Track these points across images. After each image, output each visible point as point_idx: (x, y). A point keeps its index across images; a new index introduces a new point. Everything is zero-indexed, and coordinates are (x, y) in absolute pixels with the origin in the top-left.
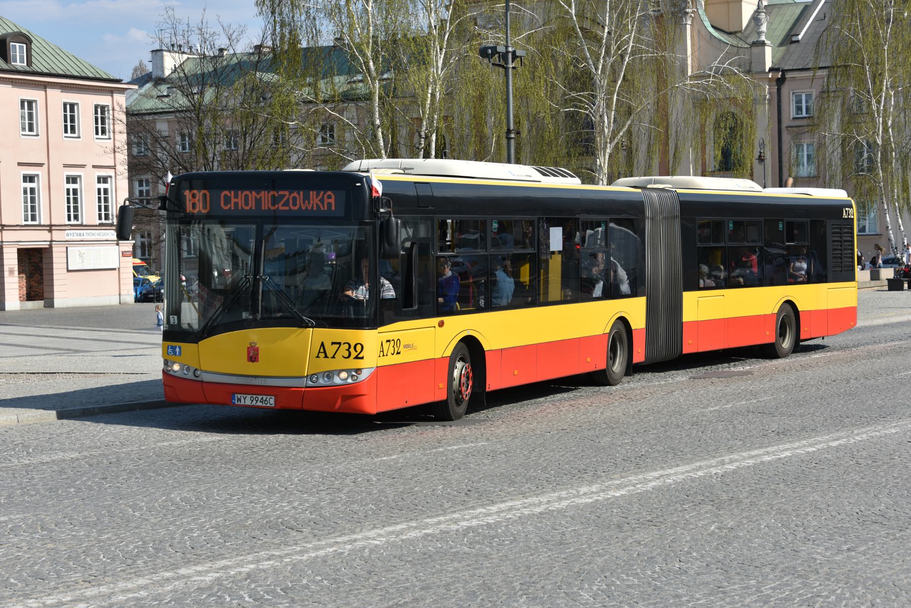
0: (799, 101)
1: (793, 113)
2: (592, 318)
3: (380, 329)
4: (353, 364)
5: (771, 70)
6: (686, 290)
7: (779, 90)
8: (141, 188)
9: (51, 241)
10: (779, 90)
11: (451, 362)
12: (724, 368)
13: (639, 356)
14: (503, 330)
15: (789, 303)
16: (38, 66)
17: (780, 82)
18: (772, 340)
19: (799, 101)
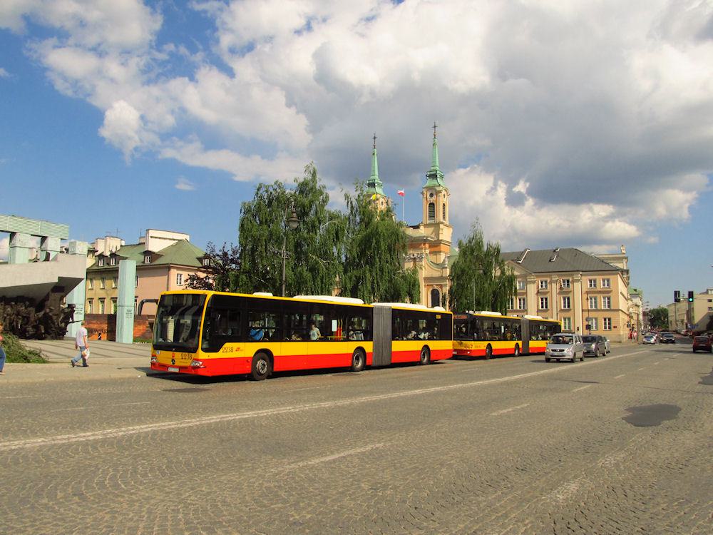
6: (393, 339)
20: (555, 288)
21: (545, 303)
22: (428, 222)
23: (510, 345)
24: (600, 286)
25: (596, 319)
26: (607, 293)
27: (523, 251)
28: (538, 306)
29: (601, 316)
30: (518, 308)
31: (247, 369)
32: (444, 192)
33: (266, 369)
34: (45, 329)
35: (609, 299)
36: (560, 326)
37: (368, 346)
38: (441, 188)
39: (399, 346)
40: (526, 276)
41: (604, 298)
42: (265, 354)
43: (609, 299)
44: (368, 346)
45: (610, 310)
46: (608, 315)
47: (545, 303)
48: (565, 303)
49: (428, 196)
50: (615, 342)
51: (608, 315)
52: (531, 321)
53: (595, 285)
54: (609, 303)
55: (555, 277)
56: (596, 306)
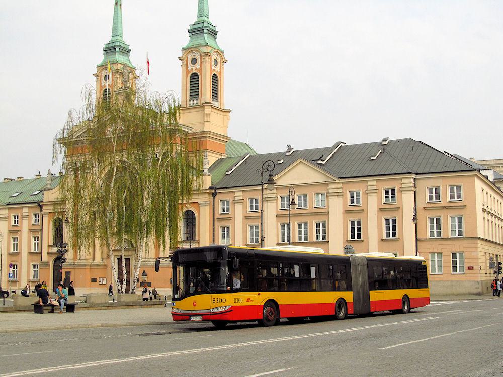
0: (352, 196)
1: (220, 212)
2: (329, 297)
3: (233, 294)
4: (222, 304)
5: (210, 188)
6: (371, 289)
7: (214, 199)
8: (35, 242)
9: (289, 214)
10: (214, 199)
11: (264, 306)
12: (388, 316)
13: (351, 311)
14: (284, 298)
15: (406, 295)
16: (81, 259)
17: (214, 194)
18: (401, 308)
19: (352, 196)
20: (373, 203)
21: (392, 228)
22: (189, 103)
23: (329, 297)
24: (445, 197)
25: (440, 254)
26: (458, 206)
27: (85, 103)
28: (345, 234)
29: (447, 249)
30: (315, 240)
31: (260, 316)
32: (214, 56)
33: (273, 315)
34: (309, 273)
35: (460, 219)
36: (425, 266)
37: (348, 296)
38: (209, 50)
39: (376, 295)
40: (328, 184)
41: (453, 217)
42: (272, 303)
43: (460, 219)
44: (348, 296)
45: (461, 237)
46: (457, 247)
47: (392, 228)
48: (432, 226)
49: (189, 62)
50: (470, 294)
51: (457, 247)
52: (370, 261)
53: (438, 197)
54: (460, 226)
55: (372, 183)
56: (439, 233)
